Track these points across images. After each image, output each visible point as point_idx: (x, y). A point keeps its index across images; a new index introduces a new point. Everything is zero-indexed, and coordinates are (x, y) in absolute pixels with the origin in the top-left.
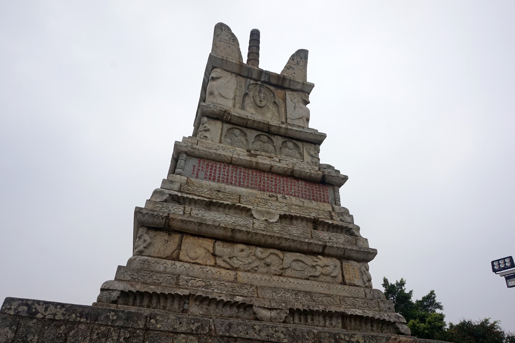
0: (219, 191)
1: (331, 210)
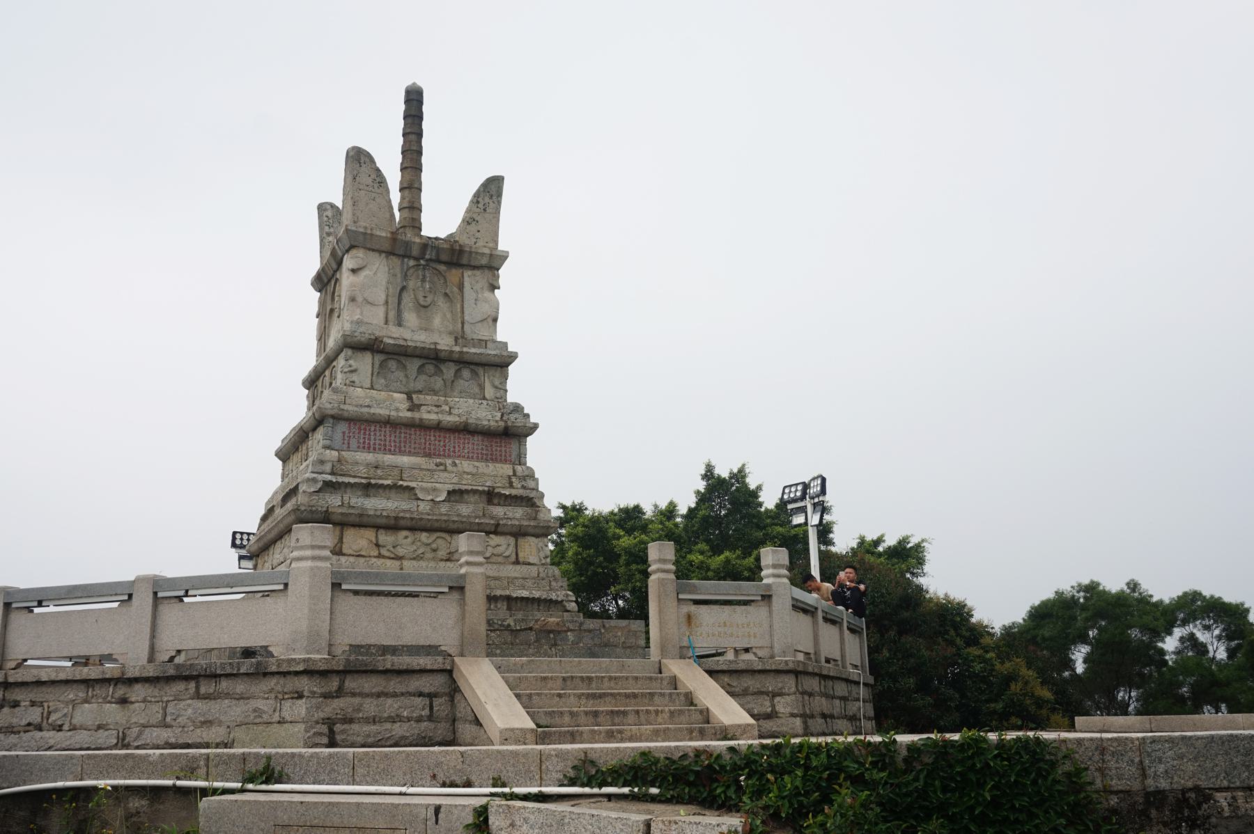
0: (376, 467)
1: (511, 474)
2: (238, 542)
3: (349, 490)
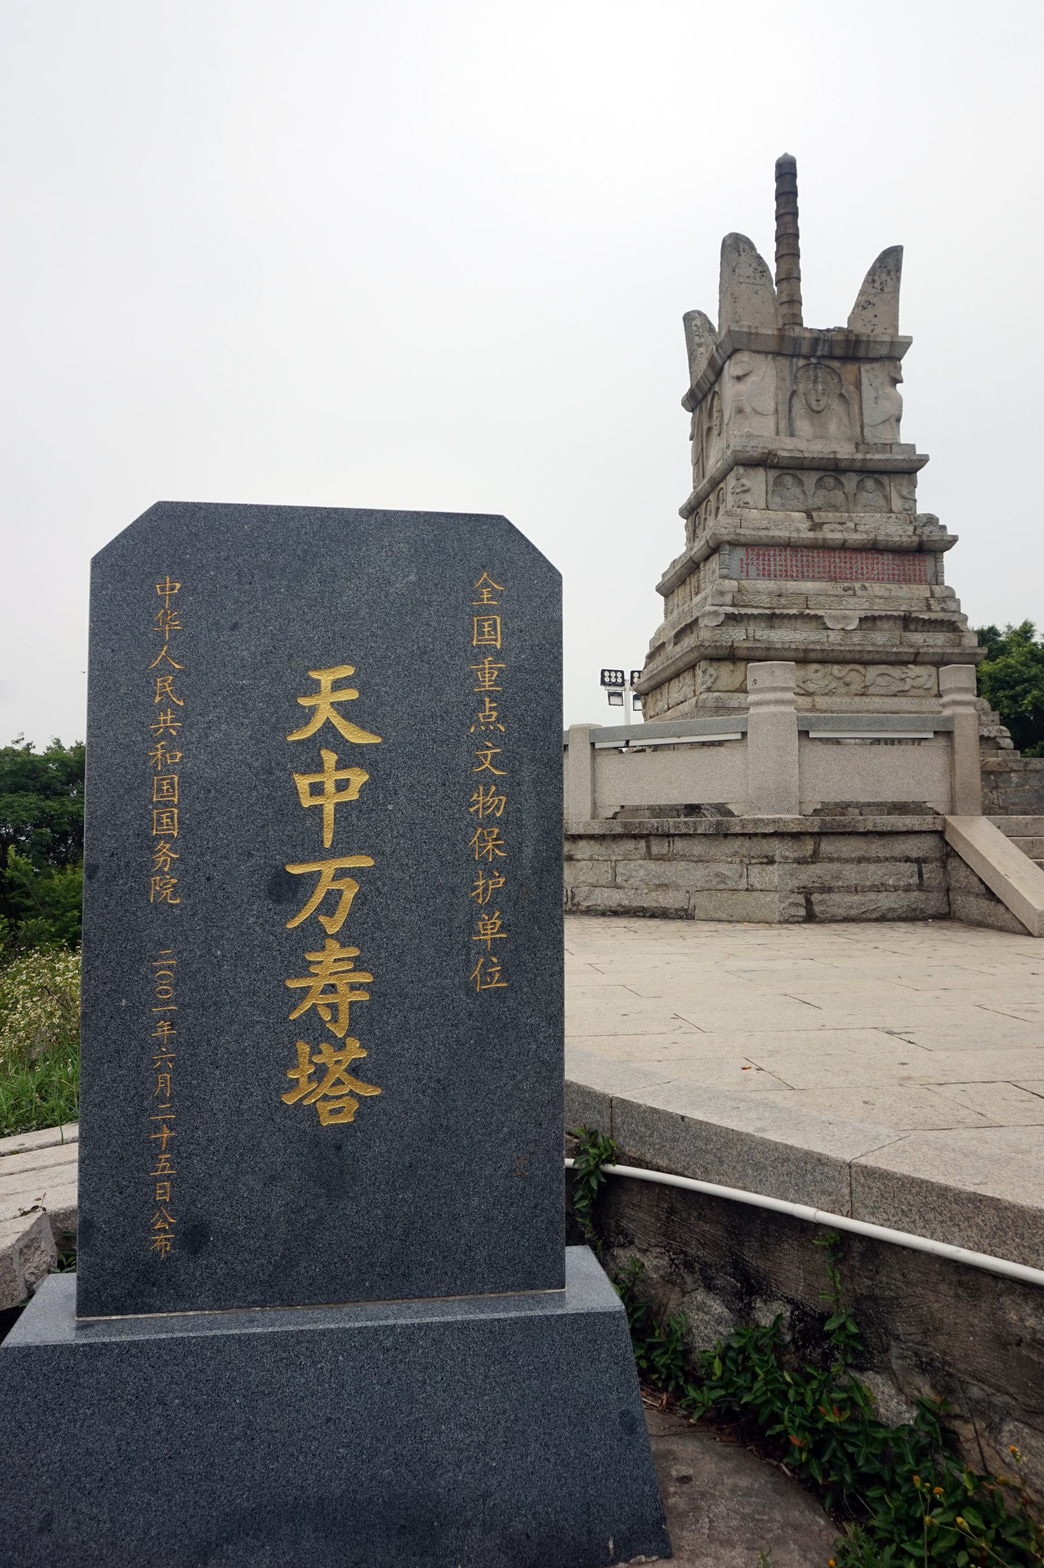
0: (779, 596)
1: (929, 595)
2: (607, 680)
3: (751, 622)
